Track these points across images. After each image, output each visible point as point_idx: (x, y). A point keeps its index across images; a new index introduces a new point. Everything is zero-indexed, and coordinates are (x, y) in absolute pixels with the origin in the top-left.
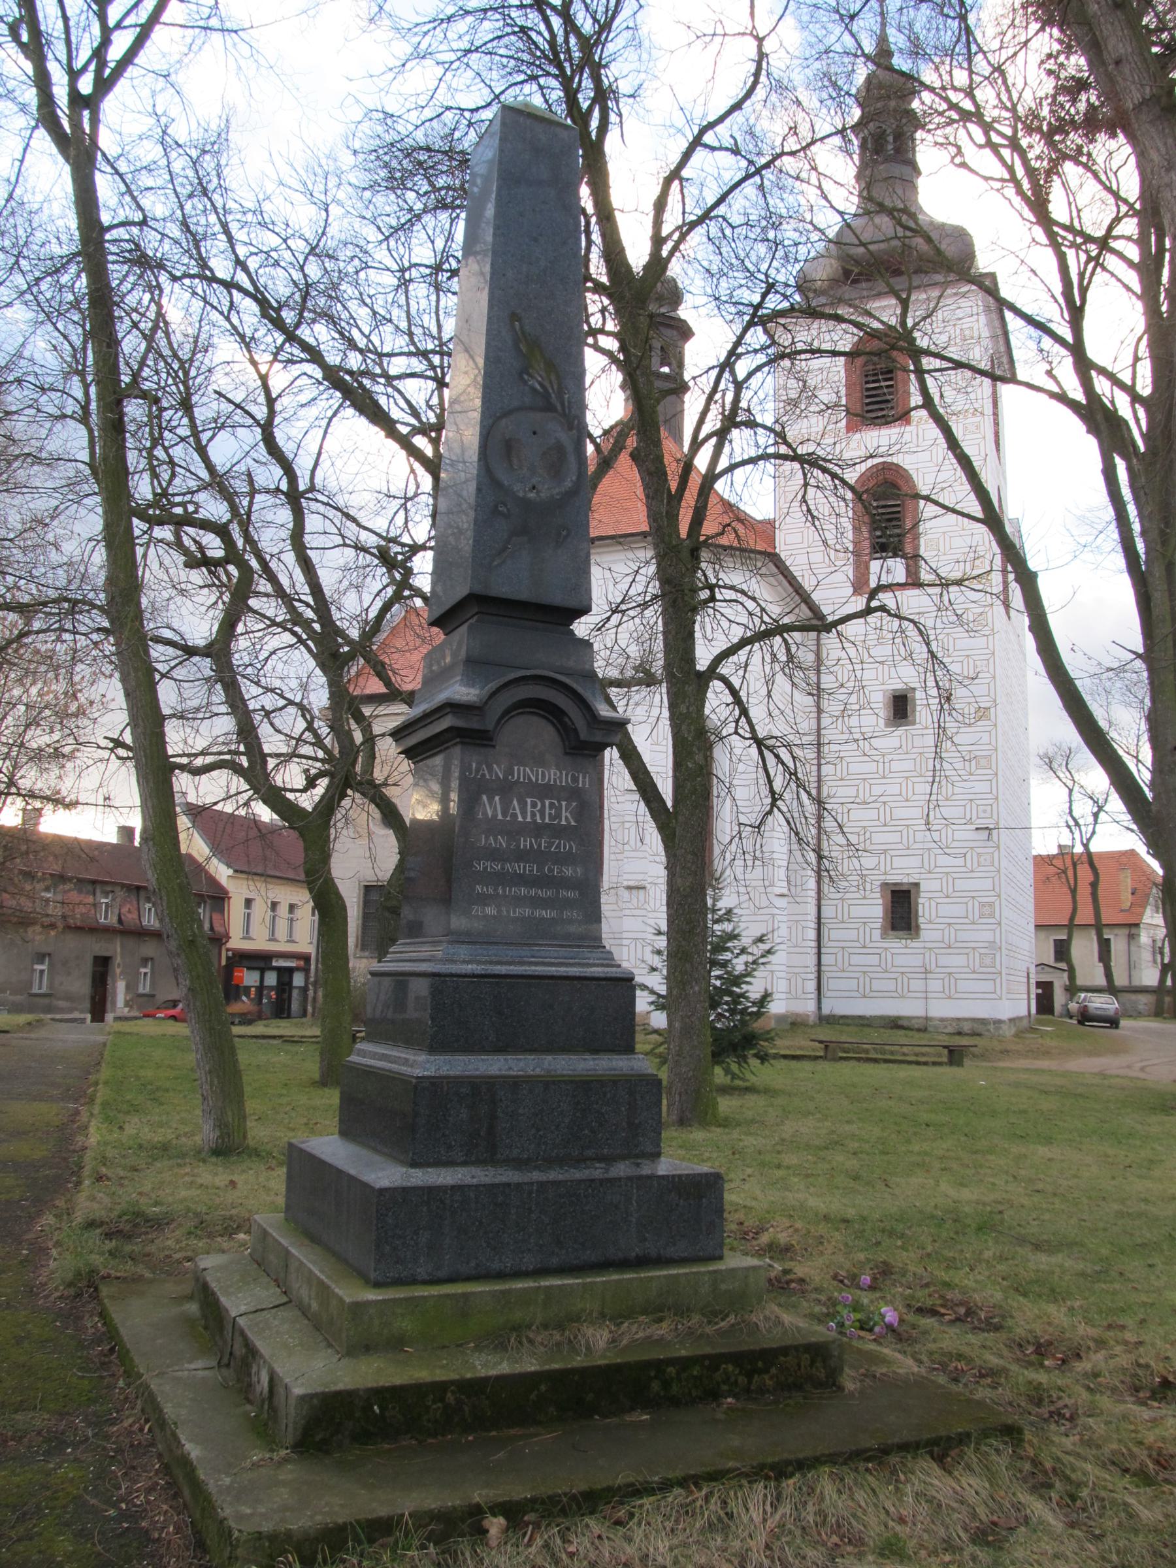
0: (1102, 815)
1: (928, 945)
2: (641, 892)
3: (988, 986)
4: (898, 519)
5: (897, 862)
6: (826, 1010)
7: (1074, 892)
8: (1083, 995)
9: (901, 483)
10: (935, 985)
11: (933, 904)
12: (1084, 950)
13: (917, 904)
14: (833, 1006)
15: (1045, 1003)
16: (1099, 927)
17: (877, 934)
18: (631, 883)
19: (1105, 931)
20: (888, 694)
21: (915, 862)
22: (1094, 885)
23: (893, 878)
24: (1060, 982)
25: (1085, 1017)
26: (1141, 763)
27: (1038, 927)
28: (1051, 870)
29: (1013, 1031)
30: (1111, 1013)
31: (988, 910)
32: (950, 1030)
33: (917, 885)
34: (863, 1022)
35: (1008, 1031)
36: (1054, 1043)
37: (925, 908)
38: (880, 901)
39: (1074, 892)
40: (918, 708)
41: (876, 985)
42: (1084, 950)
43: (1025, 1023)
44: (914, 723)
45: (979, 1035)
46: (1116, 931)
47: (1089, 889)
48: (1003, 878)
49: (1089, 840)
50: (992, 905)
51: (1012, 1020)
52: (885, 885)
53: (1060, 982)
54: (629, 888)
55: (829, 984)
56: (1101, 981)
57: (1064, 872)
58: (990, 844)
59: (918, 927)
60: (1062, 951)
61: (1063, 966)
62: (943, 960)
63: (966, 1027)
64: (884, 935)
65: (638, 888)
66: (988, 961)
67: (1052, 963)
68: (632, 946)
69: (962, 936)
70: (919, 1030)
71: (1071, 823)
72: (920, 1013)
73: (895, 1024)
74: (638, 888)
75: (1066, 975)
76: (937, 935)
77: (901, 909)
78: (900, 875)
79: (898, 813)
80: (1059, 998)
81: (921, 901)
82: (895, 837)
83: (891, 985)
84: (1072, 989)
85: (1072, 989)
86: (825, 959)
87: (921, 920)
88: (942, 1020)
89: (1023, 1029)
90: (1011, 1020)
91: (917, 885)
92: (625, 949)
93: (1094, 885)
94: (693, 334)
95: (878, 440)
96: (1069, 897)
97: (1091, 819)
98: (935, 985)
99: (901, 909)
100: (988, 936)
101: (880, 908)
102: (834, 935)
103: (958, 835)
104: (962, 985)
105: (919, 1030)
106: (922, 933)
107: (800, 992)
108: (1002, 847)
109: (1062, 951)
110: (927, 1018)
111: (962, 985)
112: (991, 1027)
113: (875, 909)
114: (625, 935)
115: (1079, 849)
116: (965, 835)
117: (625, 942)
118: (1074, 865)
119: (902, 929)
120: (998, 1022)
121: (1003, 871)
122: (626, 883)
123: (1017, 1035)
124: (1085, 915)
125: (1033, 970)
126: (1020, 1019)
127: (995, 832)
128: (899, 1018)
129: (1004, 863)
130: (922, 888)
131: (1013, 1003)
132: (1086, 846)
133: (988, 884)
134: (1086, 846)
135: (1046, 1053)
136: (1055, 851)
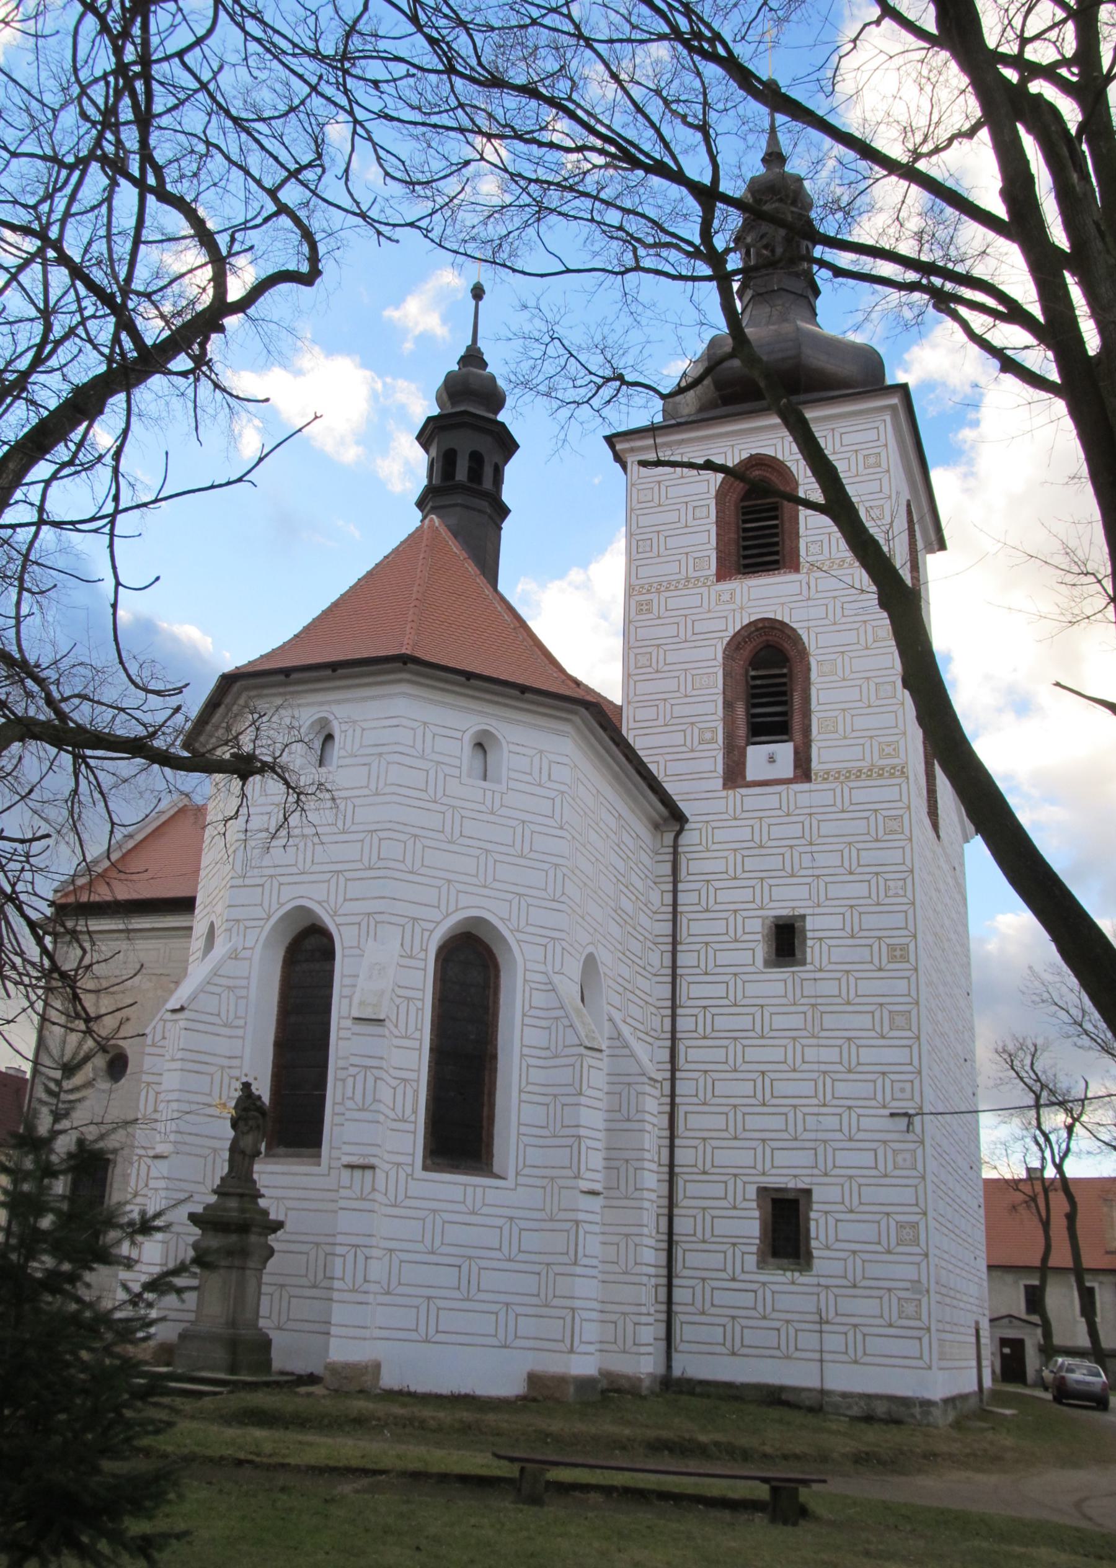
0: (1078, 1128)
1: (823, 1281)
2: (368, 1173)
3: (910, 1347)
4: (784, 693)
5: (781, 1158)
6: (677, 1372)
7: (1046, 1224)
8: (1060, 1360)
9: (787, 646)
10: (833, 1342)
11: (831, 1221)
12: (1062, 1300)
13: (808, 1220)
14: (691, 1365)
15: (1012, 1364)
16: (1079, 1272)
17: (751, 1261)
18: (355, 1160)
19: (1087, 1277)
20: (768, 922)
21: (803, 1158)
22: (1071, 1217)
23: (775, 1181)
24: (1032, 1340)
25: (1063, 1393)
26: (1111, 592)
27: (990, 1267)
28: (1020, 1197)
29: (951, 1416)
30: (1097, 1389)
31: (909, 1233)
32: (855, 1411)
33: (808, 1192)
34: (732, 1394)
35: (942, 1419)
36: (1009, 1441)
37: (820, 1227)
38: (757, 1214)
39: (1046, 1224)
40: (809, 943)
41: (750, 1337)
42: (1062, 1300)
43: (973, 1402)
44: (803, 963)
45: (898, 1422)
46: (1101, 1278)
47: (1064, 1222)
48: (930, 1187)
49: (1062, 1159)
50: (914, 1226)
51: (949, 1401)
52: (762, 1191)
53: (1032, 1340)
54: (351, 1167)
55: (684, 1333)
56: (1083, 1341)
57: (1034, 1199)
58: (911, 1137)
59: (809, 1255)
60: (1035, 1300)
61: (1035, 1319)
62: (845, 1305)
63: (881, 1409)
64: (762, 1264)
65: (364, 1167)
66: (910, 1309)
67: (1024, 1316)
68: (350, 1258)
69: (874, 1270)
70: (811, 1410)
71: (1041, 1140)
72: (813, 1382)
73: (776, 1398)
74: (364, 1167)
75: (1039, 1331)
76: (837, 1268)
77: (786, 1228)
78: (785, 1175)
79: (781, 1088)
80: (1032, 1360)
81: (813, 1215)
82: (777, 1122)
83: (771, 1339)
84: (1048, 1350)
85: (1048, 1350)
86: (679, 1295)
87: (814, 1243)
88: (844, 1395)
89: (971, 1413)
90: (947, 1401)
91: (808, 1192)
92: (338, 1261)
93: (1071, 1217)
94: (516, 446)
95: (764, 596)
96: (1040, 1233)
97: (1064, 1134)
98: (833, 1342)
99: (786, 1228)
100: (911, 1273)
101: (756, 1224)
102: (693, 1259)
103: (865, 1122)
104: (875, 1345)
105: (811, 1410)
106: (816, 1262)
107: (630, 1342)
108: (928, 1142)
109: (1035, 1300)
110: (823, 1392)
111: (875, 1345)
112: (917, 1411)
113: (750, 1226)
114: (340, 1239)
115: (1050, 1173)
116: (876, 1123)
117: (339, 1250)
118: (1046, 1191)
119: (786, 1256)
120: (927, 1404)
121: (929, 1177)
122: (346, 1159)
123: (957, 1425)
124: (1061, 1257)
125: (985, 1324)
126: (963, 1397)
127: (917, 1119)
128: (782, 1389)
129: (932, 1165)
130: (815, 1197)
131: (949, 1369)
132: (1059, 1167)
133: (908, 1195)
134: (1059, 1167)
135: (993, 1460)
136: (1023, 1175)
